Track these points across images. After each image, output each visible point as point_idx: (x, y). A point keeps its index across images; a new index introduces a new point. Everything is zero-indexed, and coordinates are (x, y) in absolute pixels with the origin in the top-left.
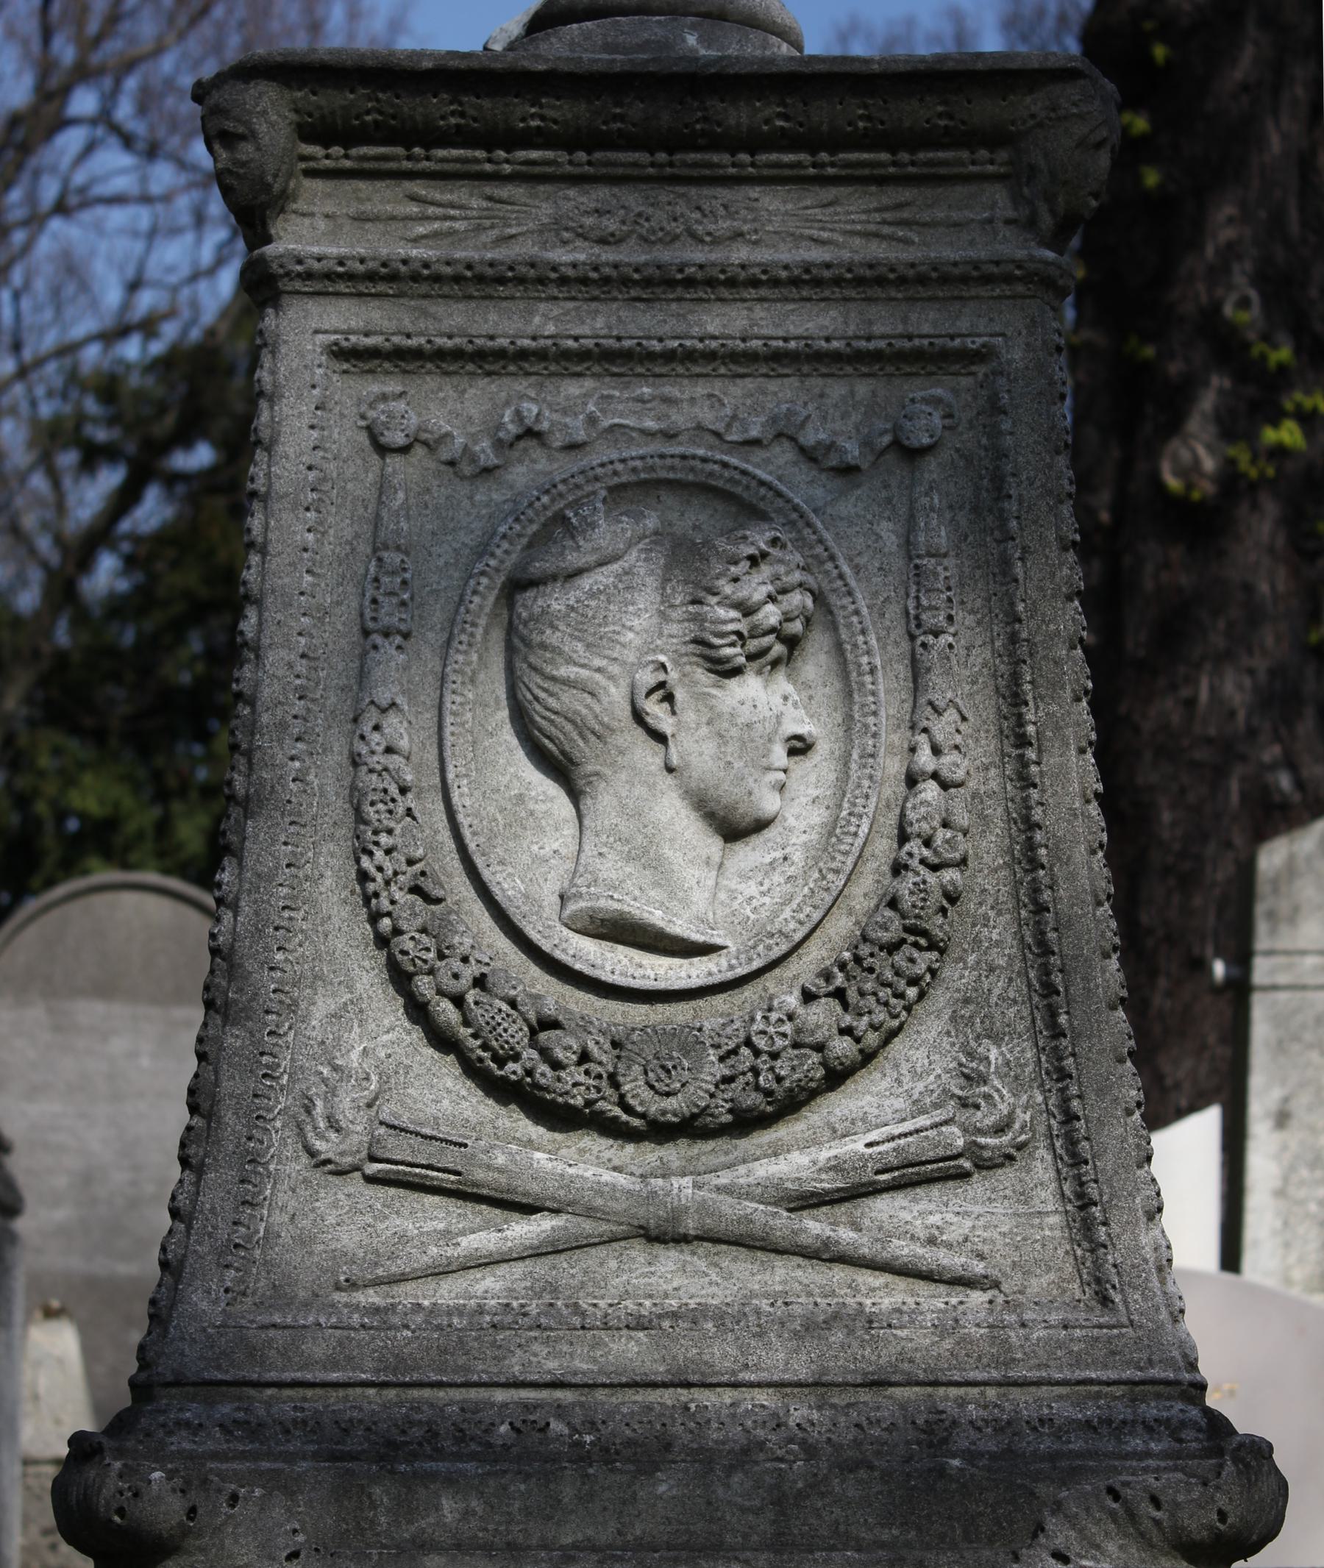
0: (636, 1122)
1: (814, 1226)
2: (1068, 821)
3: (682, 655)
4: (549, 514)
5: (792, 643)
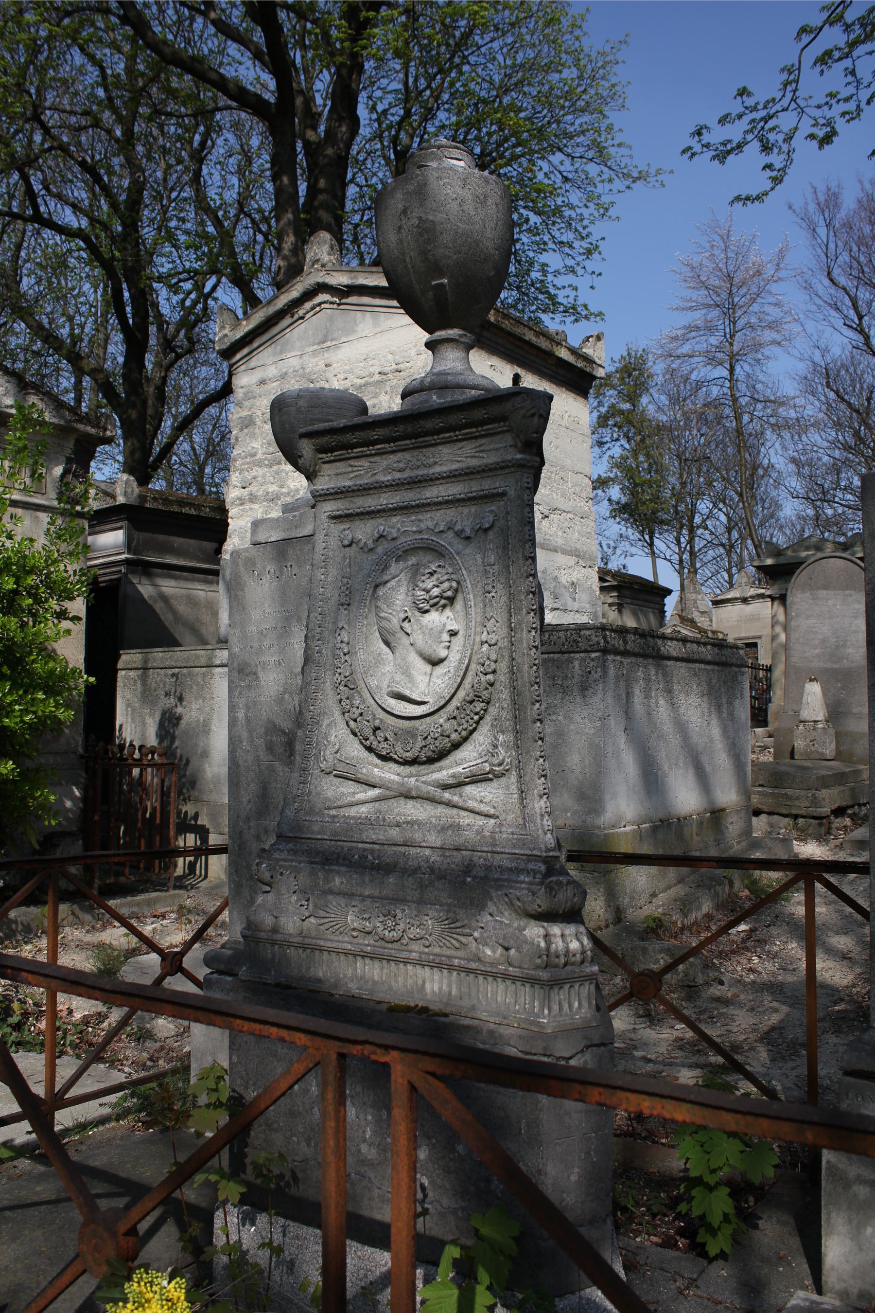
1: (447, 795)
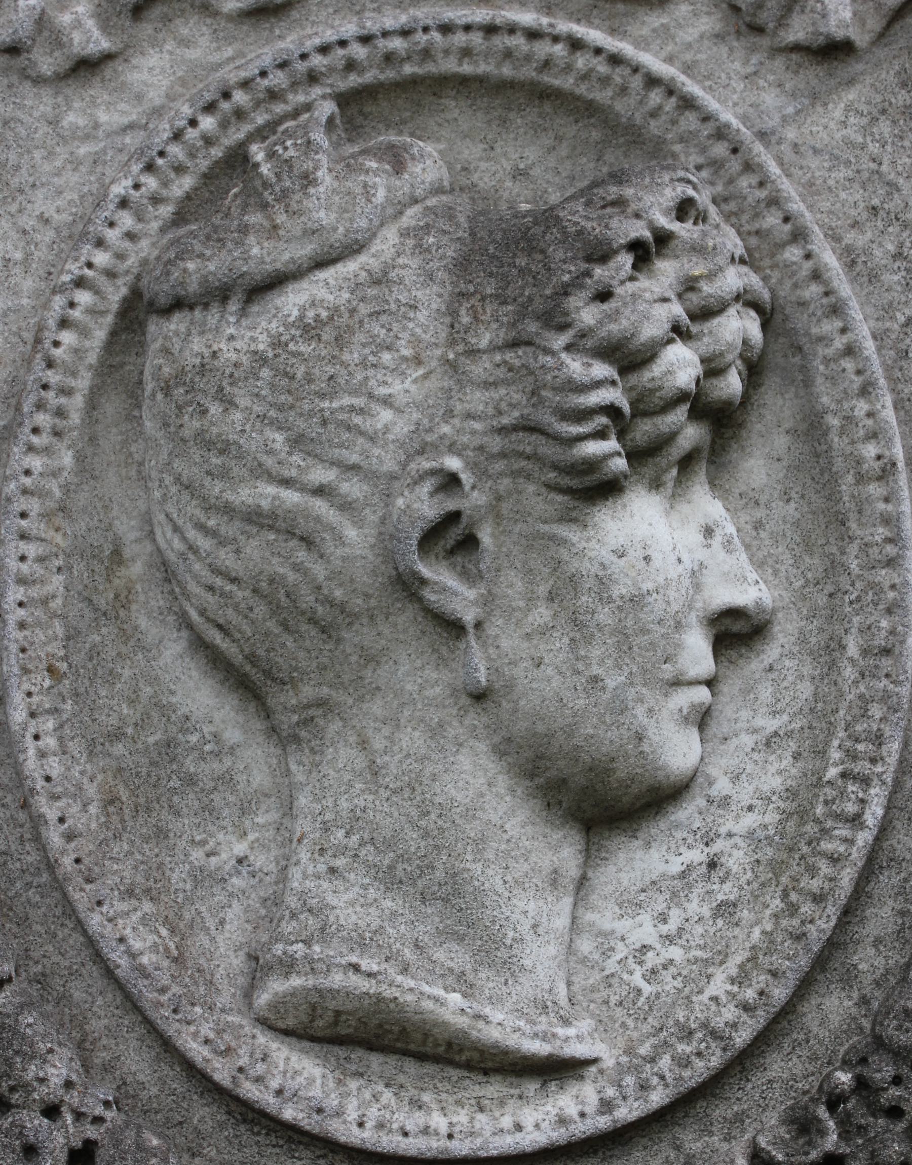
3: (493, 457)
4: (217, 152)
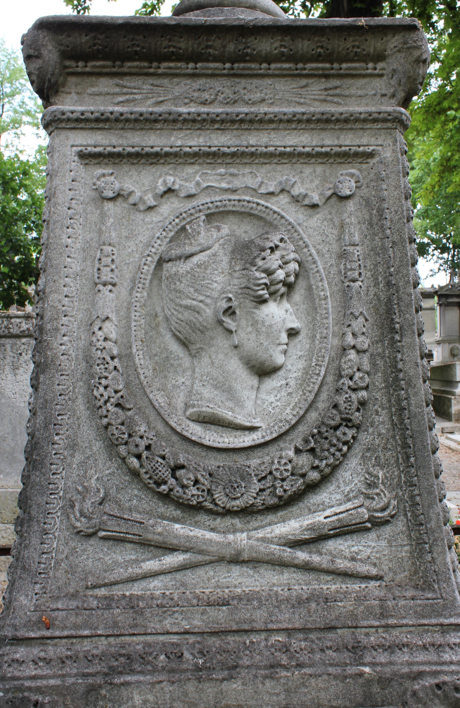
0: (221, 510)
1: (302, 556)
2: (415, 368)
3: (239, 294)
4: (179, 227)
5: (290, 286)
